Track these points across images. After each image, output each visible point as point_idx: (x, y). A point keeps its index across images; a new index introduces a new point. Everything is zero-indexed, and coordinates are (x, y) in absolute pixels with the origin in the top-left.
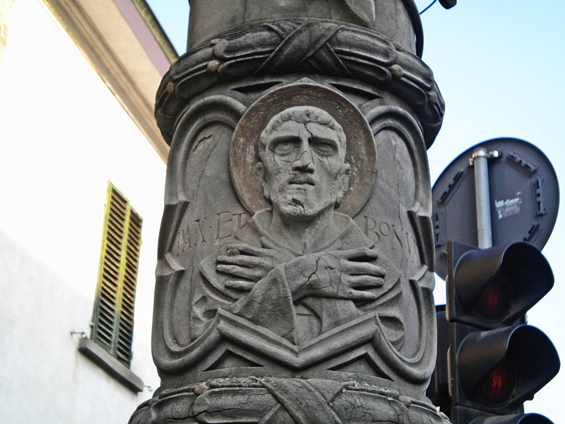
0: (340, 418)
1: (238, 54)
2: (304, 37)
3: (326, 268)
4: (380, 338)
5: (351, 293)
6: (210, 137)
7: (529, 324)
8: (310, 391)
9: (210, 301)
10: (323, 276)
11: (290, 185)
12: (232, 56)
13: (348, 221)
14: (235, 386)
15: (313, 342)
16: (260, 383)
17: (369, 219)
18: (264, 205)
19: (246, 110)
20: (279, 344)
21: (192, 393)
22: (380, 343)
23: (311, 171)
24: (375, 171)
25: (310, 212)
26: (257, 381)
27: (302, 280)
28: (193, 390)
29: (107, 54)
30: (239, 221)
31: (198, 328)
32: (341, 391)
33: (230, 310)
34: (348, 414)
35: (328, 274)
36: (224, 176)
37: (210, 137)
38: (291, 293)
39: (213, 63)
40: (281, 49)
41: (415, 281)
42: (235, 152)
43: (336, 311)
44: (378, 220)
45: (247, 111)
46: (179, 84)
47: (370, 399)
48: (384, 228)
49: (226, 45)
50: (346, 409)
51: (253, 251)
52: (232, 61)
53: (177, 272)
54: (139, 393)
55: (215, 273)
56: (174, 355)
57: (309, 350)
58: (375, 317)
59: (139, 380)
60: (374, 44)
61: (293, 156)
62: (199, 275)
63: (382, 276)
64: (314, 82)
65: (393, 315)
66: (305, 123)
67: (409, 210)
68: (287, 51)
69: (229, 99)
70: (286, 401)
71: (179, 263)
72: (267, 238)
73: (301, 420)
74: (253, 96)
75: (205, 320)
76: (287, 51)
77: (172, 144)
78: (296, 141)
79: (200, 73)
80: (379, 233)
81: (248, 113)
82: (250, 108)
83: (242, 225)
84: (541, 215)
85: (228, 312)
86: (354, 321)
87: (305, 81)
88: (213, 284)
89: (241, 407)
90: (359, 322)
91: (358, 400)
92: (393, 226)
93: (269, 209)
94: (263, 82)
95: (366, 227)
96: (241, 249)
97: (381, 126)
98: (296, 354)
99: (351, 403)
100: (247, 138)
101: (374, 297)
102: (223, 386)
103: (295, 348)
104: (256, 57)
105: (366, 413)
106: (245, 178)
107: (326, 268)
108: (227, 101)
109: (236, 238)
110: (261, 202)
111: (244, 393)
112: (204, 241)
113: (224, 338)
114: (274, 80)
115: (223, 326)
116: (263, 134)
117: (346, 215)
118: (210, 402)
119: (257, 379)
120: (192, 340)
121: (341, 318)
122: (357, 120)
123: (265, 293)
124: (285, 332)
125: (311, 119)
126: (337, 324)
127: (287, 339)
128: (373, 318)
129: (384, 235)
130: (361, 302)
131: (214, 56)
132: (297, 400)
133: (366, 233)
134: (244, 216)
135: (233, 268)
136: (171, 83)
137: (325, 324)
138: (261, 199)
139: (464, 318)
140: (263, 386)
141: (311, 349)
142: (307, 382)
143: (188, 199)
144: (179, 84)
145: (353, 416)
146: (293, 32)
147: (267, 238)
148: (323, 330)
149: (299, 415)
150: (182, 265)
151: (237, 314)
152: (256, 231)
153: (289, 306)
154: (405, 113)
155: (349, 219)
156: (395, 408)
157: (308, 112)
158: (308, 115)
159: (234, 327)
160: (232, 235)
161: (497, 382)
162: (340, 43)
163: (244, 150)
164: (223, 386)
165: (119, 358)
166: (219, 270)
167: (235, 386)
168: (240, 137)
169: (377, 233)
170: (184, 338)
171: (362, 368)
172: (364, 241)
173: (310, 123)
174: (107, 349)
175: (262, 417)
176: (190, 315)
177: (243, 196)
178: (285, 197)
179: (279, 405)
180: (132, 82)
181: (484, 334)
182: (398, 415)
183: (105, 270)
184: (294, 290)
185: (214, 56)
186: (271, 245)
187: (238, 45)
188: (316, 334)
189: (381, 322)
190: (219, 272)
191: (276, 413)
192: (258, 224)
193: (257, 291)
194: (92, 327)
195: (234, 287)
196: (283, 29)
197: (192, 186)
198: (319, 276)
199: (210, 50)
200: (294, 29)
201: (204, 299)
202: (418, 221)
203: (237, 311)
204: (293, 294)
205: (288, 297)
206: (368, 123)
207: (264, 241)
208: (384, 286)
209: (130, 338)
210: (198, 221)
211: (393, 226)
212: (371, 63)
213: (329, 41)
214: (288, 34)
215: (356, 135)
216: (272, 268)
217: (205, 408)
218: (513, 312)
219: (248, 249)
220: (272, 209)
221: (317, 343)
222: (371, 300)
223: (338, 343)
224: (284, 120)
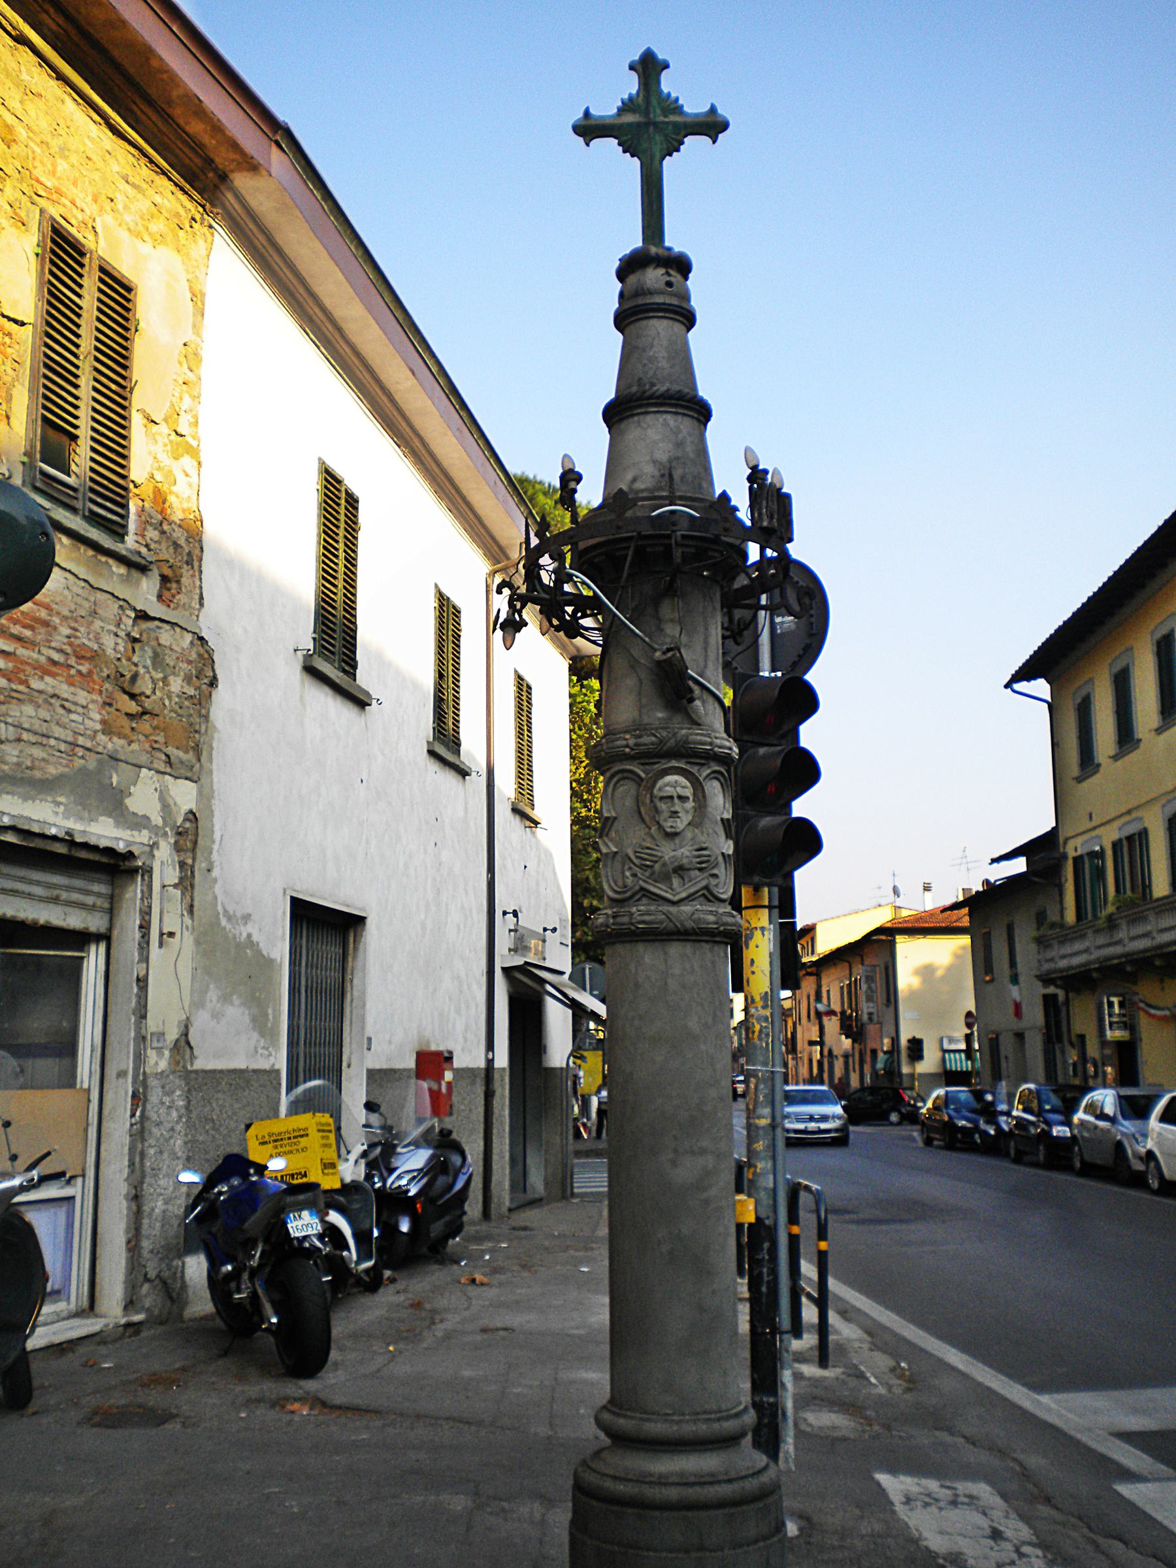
2: (672, 741)
7: (808, 677)
10: (685, 861)
29: (310, 301)
39: (627, 750)
54: (367, 708)
59: (368, 694)
69: (637, 770)
78: (671, 797)
84: (813, 635)
113: (642, 889)
115: (641, 883)
118: (639, 918)
130: (700, 870)
131: (627, 746)
139: (745, 738)
152: (653, 837)
161: (771, 788)
165: (344, 671)
170: (620, 883)
174: (331, 663)
180: (339, 329)
181: (762, 751)
183: (324, 570)
185: (627, 746)
194: (314, 639)
209: (355, 646)
218: (786, 728)
223: (692, 890)
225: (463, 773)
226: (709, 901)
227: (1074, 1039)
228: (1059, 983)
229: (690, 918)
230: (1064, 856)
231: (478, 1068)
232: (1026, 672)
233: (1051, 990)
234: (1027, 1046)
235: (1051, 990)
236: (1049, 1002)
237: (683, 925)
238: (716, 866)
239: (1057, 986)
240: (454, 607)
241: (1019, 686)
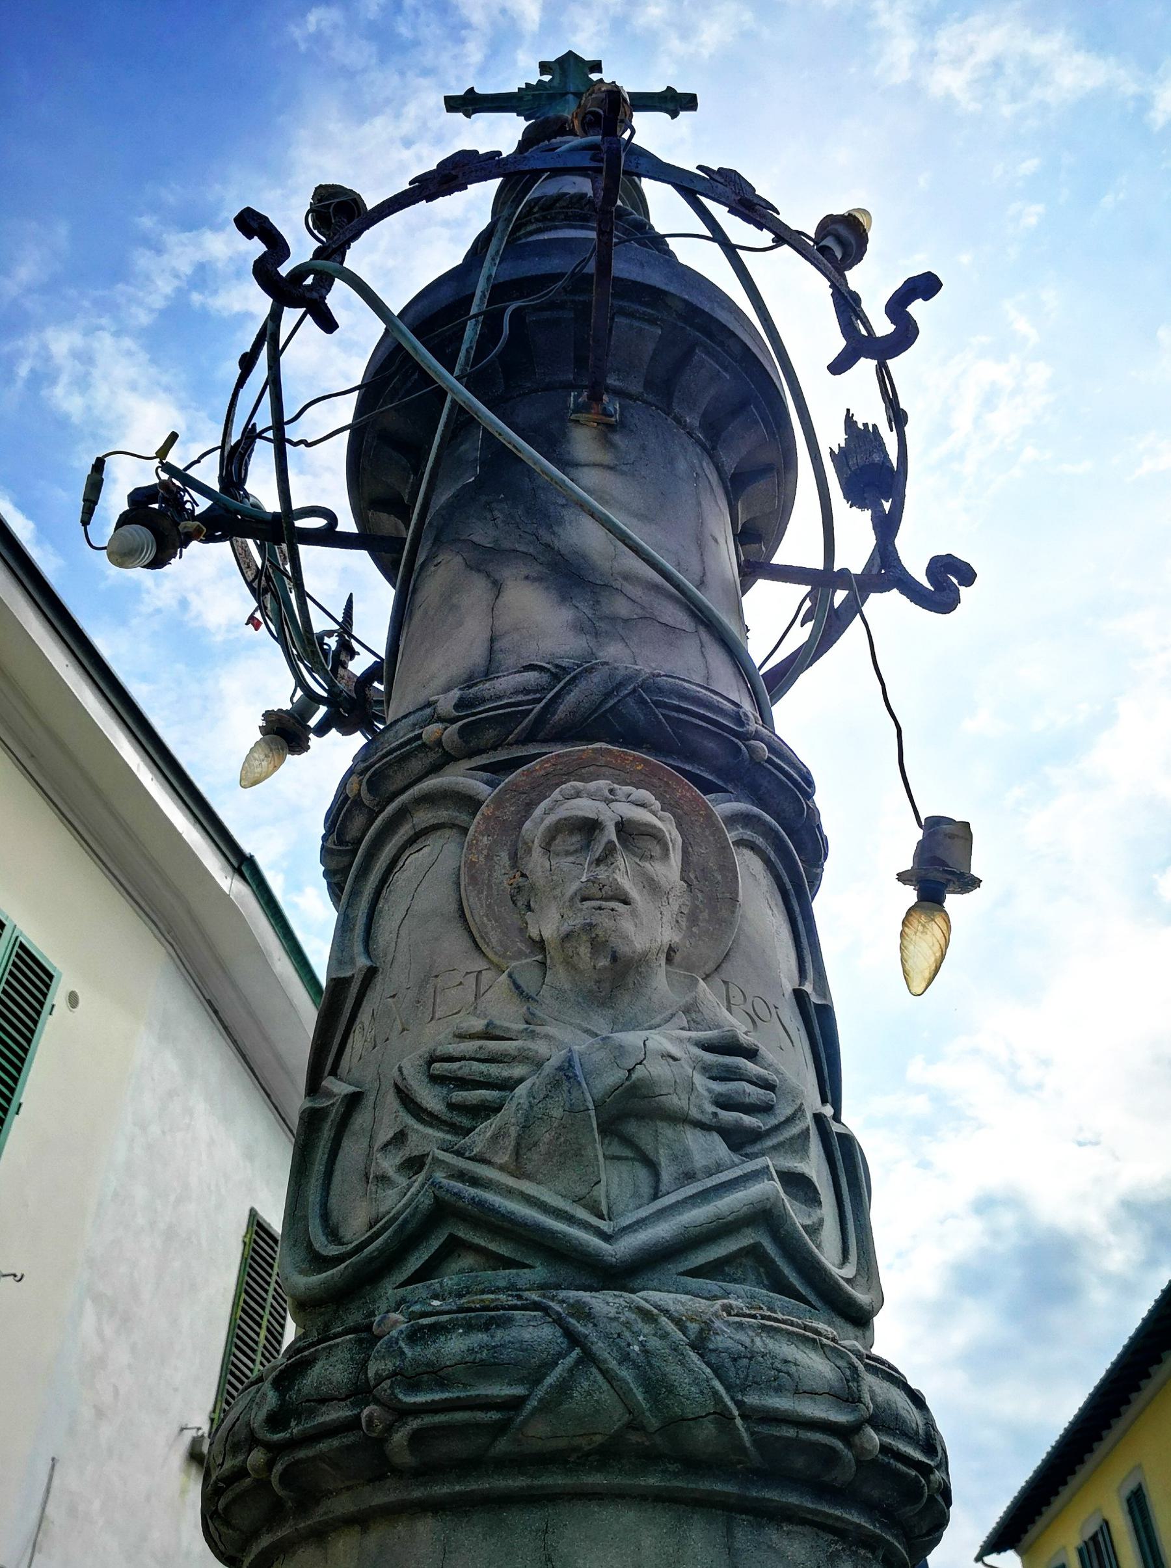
0: (722, 1383)
9: (413, 1139)
10: (656, 1069)
15: (643, 1213)
18: (528, 951)
20: (570, 1219)
34: (740, 1372)
40: (558, 695)
41: (825, 1116)
43: (687, 1153)
46: (367, 776)
47: (784, 1340)
50: (735, 1360)
53: (346, 1096)
75: (402, 1181)
77: (398, 584)
80: (752, 1013)
91: (758, 1340)
92: (776, 1008)
93: (539, 957)
98: (607, 1237)
103: (604, 1225)
106: (489, 906)
124: (581, 1190)
125: (617, 797)
126: (689, 1176)
127: (585, 1206)
128: (764, 1168)
133: (729, 1010)
137: (666, 1176)
148: (663, 1188)
155: (698, 980)
182: (848, 1381)
188: (645, 1200)
201: (400, 1138)
202: (813, 1011)
211: (776, 1008)
222: (756, 1136)
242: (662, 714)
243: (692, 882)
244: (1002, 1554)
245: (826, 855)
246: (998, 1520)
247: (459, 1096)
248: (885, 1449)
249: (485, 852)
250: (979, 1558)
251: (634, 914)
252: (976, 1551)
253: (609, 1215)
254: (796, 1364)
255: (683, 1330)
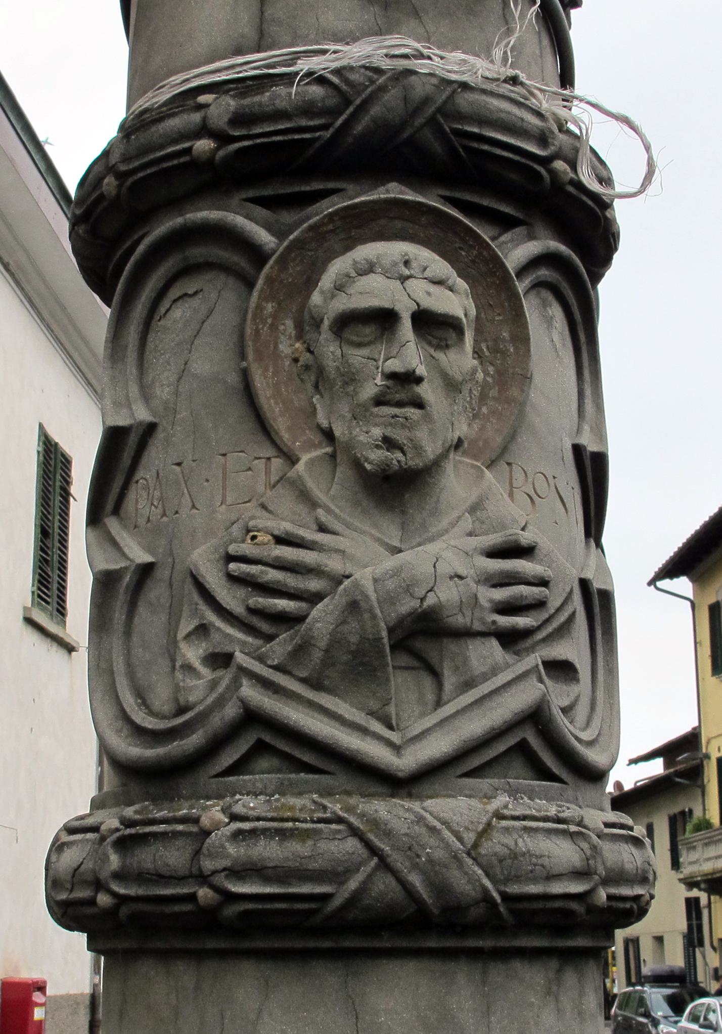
1: (258, 130)
3: (451, 578)
4: (550, 710)
5: (494, 622)
6: (196, 293)
8: (432, 830)
9: (216, 637)
11: (376, 409)
12: (244, 132)
13: (481, 476)
14: (283, 820)
16: (334, 813)
17: (514, 466)
19: (278, 246)
20: (364, 731)
21: (194, 829)
22: (550, 718)
23: (419, 380)
24: (529, 376)
25: (415, 462)
26: (325, 808)
27: (407, 606)
28: (196, 821)
30: (268, 472)
31: (192, 687)
32: (489, 825)
33: (261, 659)
35: (456, 589)
36: (233, 379)
37: (196, 293)
38: (386, 630)
39: (204, 145)
40: (347, 124)
42: (257, 332)
44: (529, 470)
45: (281, 249)
46: (130, 180)
48: (540, 483)
49: (232, 109)
50: (501, 861)
51: (303, 538)
52: (246, 143)
55: (224, 578)
56: (139, 732)
57: (421, 740)
58: (537, 666)
60: (522, 119)
61: (381, 351)
62: (189, 580)
63: (544, 583)
64: (412, 192)
65: (563, 657)
66: (403, 279)
67: (576, 441)
68: (359, 128)
69: (239, 221)
70: (390, 852)
71: (139, 543)
72: (329, 511)
73: (419, 888)
74: (287, 217)
75: (204, 671)
76: (359, 128)
79: (175, 162)
80: (532, 493)
81: (282, 254)
82: (286, 244)
83: (273, 481)
85: (257, 663)
86: (500, 676)
87: (394, 191)
88: (222, 602)
89: (300, 863)
90: (509, 678)
91: (520, 841)
92: (554, 477)
94: (308, 188)
95: (511, 484)
96: (276, 532)
97: (531, 281)
98: (397, 749)
99: (507, 847)
100: (279, 304)
101: (533, 626)
102: (258, 819)
103: (394, 737)
104: (296, 137)
105: (535, 865)
106: (276, 386)
107: (451, 578)
108: (236, 226)
109: (264, 507)
110: (316, 437)
111: (305, 835)
112: (194, 507)
114: (331, 185)
115: (249, 692)
116: (316, 298)
117: (476, 463)
119: (325, 802)
120: (182, 710)
121: (477, 672)
122: (495, 272)
123: (333, 630)
124: (374, 705)
126: (468, 685)
128: (533, 668)
129: (540, 497)
131: (204, 131)
132: (410, 848)
133: (511, 495)
134: (277, 463)
135: (262, 572)
136: (113, 179)
138: (310, 429)
140: (340, 820)
141: (426, 737)
142: (423, 808)
143: (155, 417)
144: (130, 180)
145: (513, 873)
146: (370, 89)
147: (329, 511)
148: (445, 698)
149: (415, 880)
150: (149, 550)
151: (277, 668)
152: (305, 497)
153: (382, 655)
154: (570, 255)
155: (482, 470)
156: (582, 846)
157: (407, 257)
158: (407, 263)
159: (270, 693)
160: (254, 500)
162: (461, 117)
163: (273, 327)
164: (258, 819)
166: (232, 573)
167: (283, 820)
168: (267, 302)
169: (528, 495)
171: (518, 765)
172: (510, 513)
173: (411, 280)
175: (342, 883)
176: (173, 660)
177: (275, 419)
178: (367, 433)
179: (375, 860)
182: (588, 860)
184: (391, 625)
185: (204, 131)
186: (337, 526)
187: (256, 109)
188: (430, 706)
189: (547, 674)
190: (234, 579)
191: (370, 877)
192: (310, 484)
193: (319, 625)
195: (267, 611)
196: (347, 82)
197: (163, 393)
198: (440, 595)
199: (196, 117)
200: (372, 82)
201: (203, 630)
202: (588, 463)
203: (276, 662)
204: (391, 631)
205: (383, 638)
206: (514, 276)
207: (323, 519)
208: (549, 605)
210: (179, 464)
211: (554, 477)
212: (516, 158)
213: (439, 110)
214: (359, 94)
215: (492, 303)
216: (348, 577)
217: (227, 863)
219: (292, 534)
220: (335, 452)
221: (435, 726)
222: (527, 633)
224: (361, 272)
225: (70, 649)
226: (546, 775)
227: (716, 943)
228: (703, 886)
229: (473, 851)
230: (707, 756)
231: (82, 994)
232: (672, 569)
233: (695, 893)
234: (666, 953)
235: (695, 893)
236: (692, 906)
237: (441, 889)
238: (564, 630)
239: (700, 890)
240: (63, 455)
241: (664, 584)
242: (461, 145)
243: (483, 353)
244: (675, 580)
245: (616, 249)
246: (676, 549)
247: (262, 601)
248: (610, 897)
249: (269, 321)
250: (652, 582)
251: (428, 418)
252: (651, 575)
253: (397, 725)
254: (549, 857)
255: (460, 839)
